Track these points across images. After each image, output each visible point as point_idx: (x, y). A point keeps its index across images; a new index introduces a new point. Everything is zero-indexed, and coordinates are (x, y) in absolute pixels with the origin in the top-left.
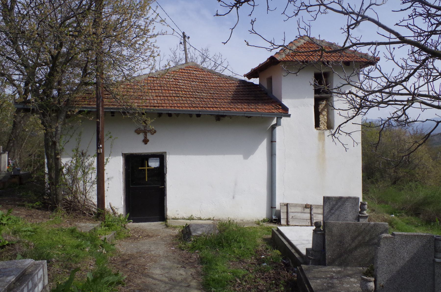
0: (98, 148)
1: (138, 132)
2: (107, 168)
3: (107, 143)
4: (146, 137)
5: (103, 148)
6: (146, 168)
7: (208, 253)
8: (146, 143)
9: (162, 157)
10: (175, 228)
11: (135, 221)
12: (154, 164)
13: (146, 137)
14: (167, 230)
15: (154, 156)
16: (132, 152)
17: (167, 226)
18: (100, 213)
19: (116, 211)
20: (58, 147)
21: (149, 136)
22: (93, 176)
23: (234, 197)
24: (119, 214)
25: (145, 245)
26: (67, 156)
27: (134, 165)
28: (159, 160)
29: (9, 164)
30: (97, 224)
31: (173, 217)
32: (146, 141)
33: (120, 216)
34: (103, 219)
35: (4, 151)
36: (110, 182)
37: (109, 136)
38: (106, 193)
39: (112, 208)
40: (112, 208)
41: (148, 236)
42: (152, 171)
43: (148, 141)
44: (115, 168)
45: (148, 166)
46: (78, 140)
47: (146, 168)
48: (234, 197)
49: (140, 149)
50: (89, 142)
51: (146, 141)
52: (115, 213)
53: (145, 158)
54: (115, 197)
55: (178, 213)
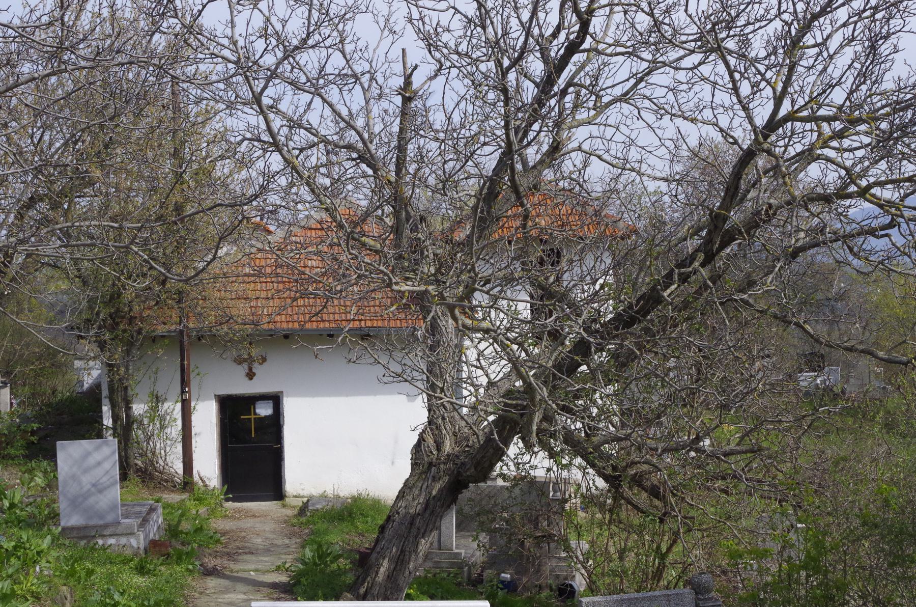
0: (183, 392)
1: (239, 361)
2: (196, 419)
3: (194, 383)
4: (250, 369)
5: (189, 392)
6: (253, 417)
7: (322, 526)
8: (251, 379)
9: (276, 400)
10: (294, 507)
11: (234, 500)
12: (264, 410)
13: (250, 369)
14: (284, 510)
15: (264, 397)
16: (230, 393)
17: (284, 506)
18: (187, 484)
19: (208, 482)
20: (130, 392)
21: (257, 369)
22: (175, 430)
23: (393, 463)
24: (212, 487)
25: (248, 523)
26: (142, 402)
27: (233, 409)
28: (271, 405)
29: (11, 404)
30: (184, 496)
31: (295, 494)
32: (251, 375)
33: (213, 490)
34: (192, 490)
35: (5, 384)
36: (198, 439)
37: (196, 371)
38: (195, 456)
39: (201, 479)
40: (201, 479)
41: (254, 516)
42: (261, 420)
43: (254, 374)
44: (206, 418)
45: (255, 414)
46: (152, 379)
47: (253, 417)
48: (393, 463)
49: (241, 387)
50: (170, 381)
51: (251, 375)
52: (206, 486)
53: (250, 401)
54: (208, 464)
55: (302, 487)
